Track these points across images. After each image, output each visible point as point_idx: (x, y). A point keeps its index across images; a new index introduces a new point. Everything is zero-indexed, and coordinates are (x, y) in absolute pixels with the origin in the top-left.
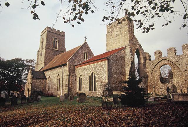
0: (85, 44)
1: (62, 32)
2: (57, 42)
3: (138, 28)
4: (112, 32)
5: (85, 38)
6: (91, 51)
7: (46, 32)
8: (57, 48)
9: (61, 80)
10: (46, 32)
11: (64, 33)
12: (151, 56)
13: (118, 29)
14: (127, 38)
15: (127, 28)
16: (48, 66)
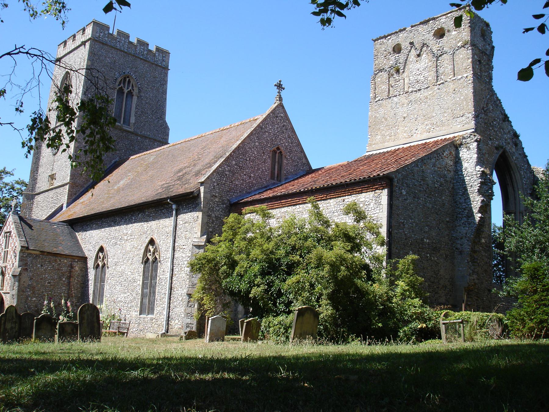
0: (279, 118)
1: (158, 49)
2: (130, 94)
3: (532, 29)
4: (398, 71)
5: (279, 86)
6: (299, 144)
7: (88, 44)
8: (133, 120)
9: (164, 270)
10: (84, 43)
11: (164, 54)
12: (493, 27)
13: (426, 60)
14: (465, 99)
15: (465, 58)
16: (84, 207)
